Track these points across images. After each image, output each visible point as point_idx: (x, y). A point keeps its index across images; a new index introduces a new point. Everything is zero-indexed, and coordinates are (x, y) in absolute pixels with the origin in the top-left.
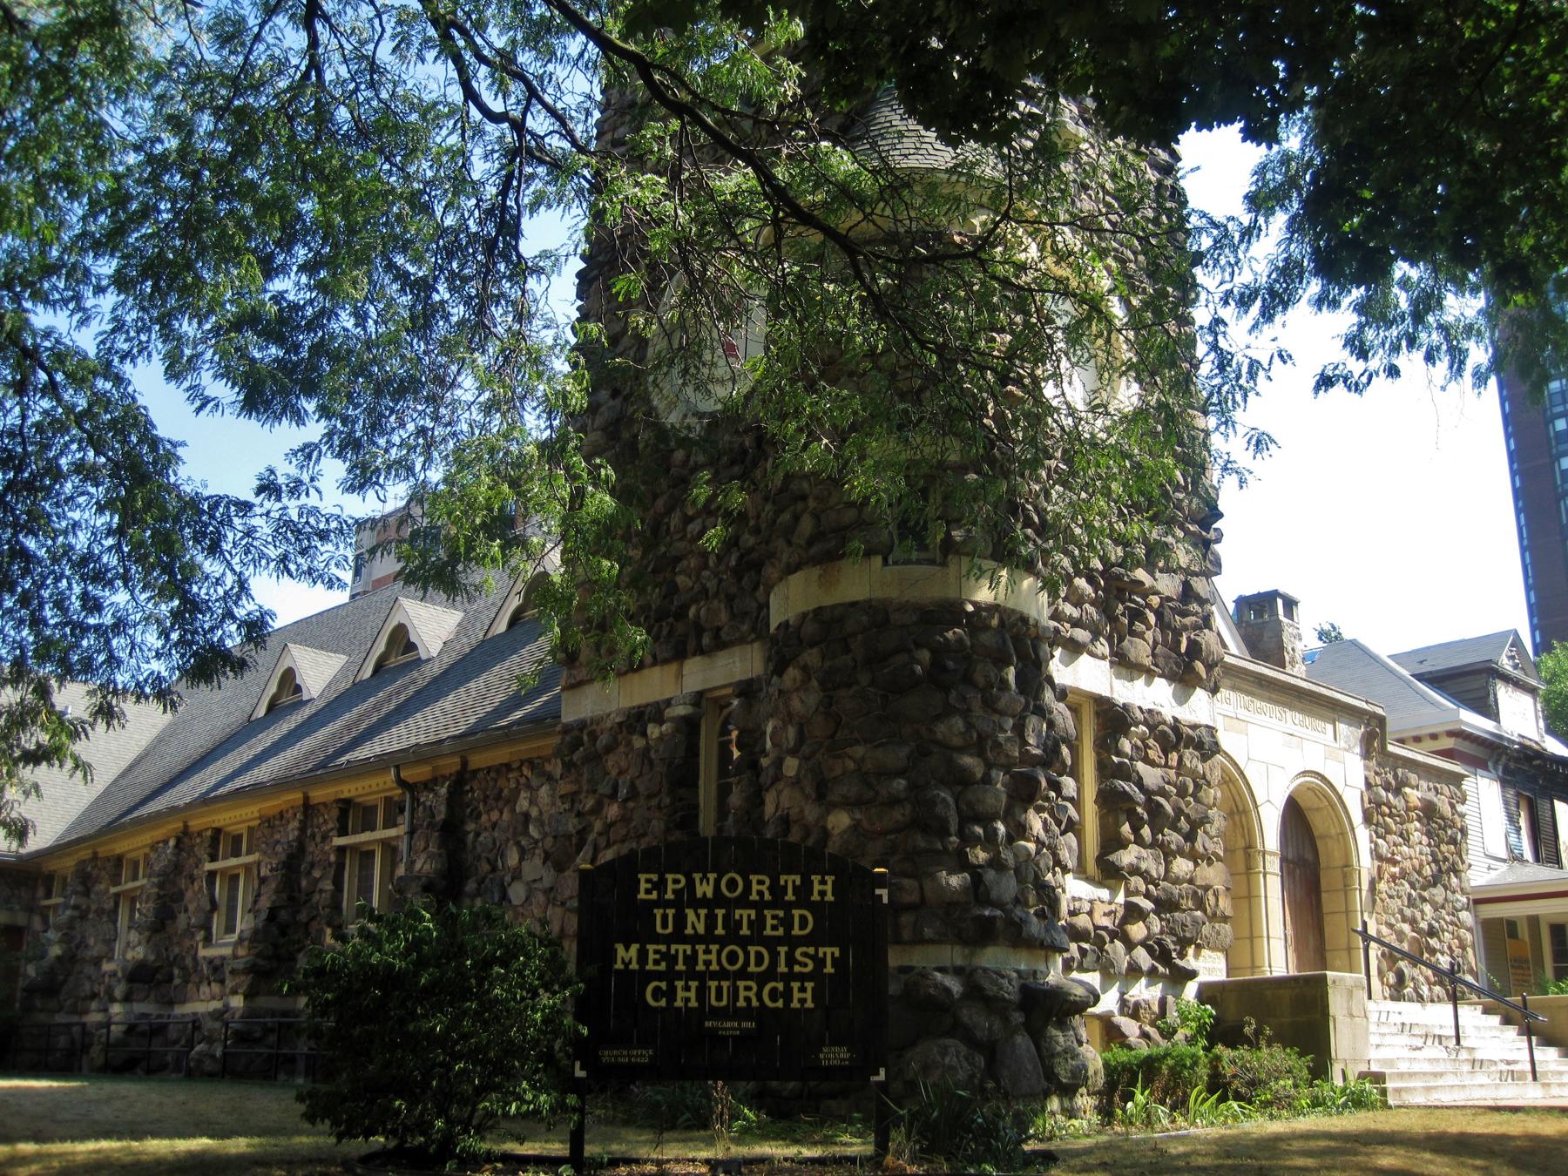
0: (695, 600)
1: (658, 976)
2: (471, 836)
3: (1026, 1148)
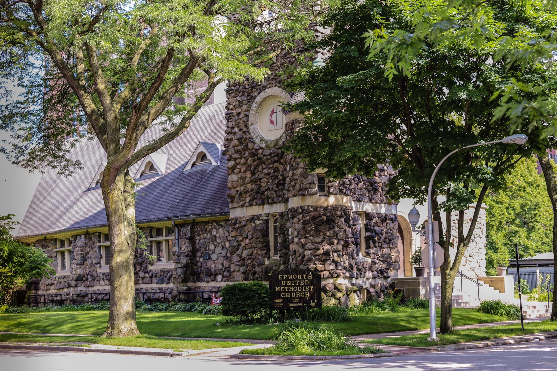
0: (266, 190)
1: (283, 292)
3: (406, 129)
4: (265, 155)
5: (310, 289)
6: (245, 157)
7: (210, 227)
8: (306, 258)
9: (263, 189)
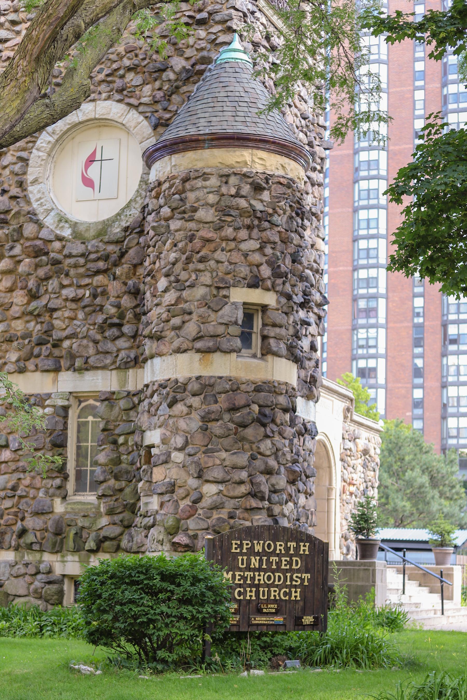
0: (67, 338)
1: (240, 586)
4: (70, 256)
6: (11, 257)
8: (206, 502)
9: (56, 335)
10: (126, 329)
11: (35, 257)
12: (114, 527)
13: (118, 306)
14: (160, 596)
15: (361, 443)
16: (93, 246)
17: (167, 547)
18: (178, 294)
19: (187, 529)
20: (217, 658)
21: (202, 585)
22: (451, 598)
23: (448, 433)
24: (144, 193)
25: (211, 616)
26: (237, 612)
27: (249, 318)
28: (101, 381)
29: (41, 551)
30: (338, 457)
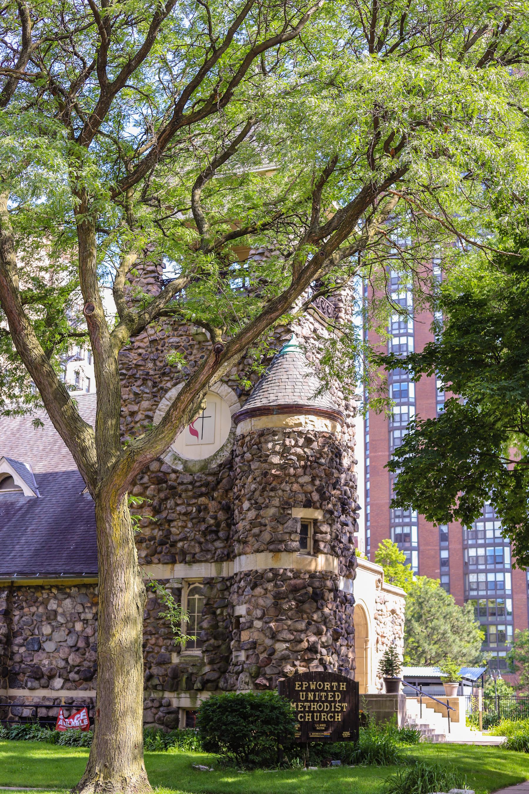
0: (181, 540)
1: (301, 712)
2: (17, 618)
4: (182, 483)
5: (342, 708)
6: (142, 484)
7: (45, 596)
8: (277, 656)
10: (221, 534)
11: (158, 484)
12: (214, 673)
13: (215, 518)
14: (250, 719)
15: (390, 606)
16: (198, 477)
17: (251, 686)
18: (257, 512)
19: (265, 674)
20: (286, 759)
21: (277, 712)
22: (457, 721)
23: (469, 586)
24: (232, 441)
25: (283, 732)
26: (300, 730)
27: (305, 528)
28: (204, 571)
29: (163, 690)
30: (372, 617)
